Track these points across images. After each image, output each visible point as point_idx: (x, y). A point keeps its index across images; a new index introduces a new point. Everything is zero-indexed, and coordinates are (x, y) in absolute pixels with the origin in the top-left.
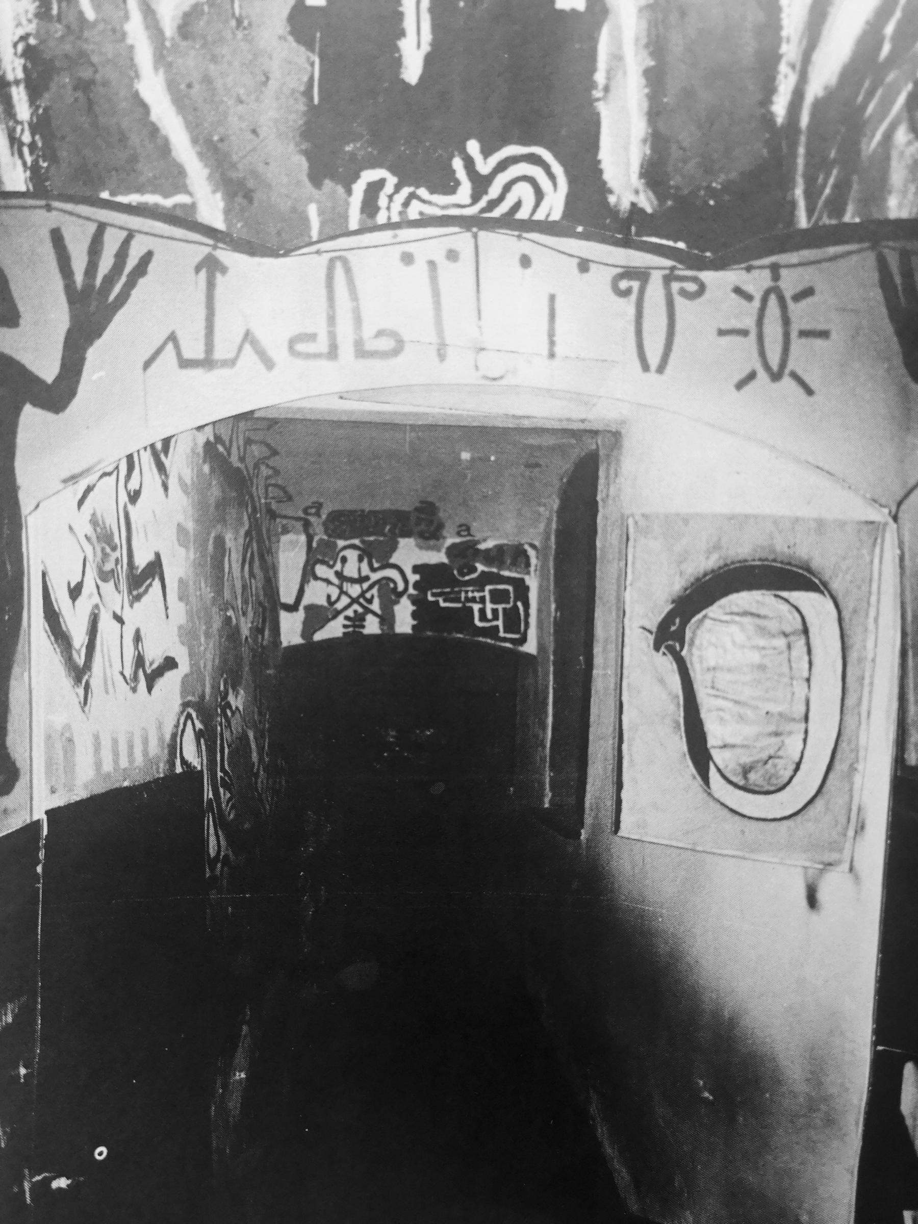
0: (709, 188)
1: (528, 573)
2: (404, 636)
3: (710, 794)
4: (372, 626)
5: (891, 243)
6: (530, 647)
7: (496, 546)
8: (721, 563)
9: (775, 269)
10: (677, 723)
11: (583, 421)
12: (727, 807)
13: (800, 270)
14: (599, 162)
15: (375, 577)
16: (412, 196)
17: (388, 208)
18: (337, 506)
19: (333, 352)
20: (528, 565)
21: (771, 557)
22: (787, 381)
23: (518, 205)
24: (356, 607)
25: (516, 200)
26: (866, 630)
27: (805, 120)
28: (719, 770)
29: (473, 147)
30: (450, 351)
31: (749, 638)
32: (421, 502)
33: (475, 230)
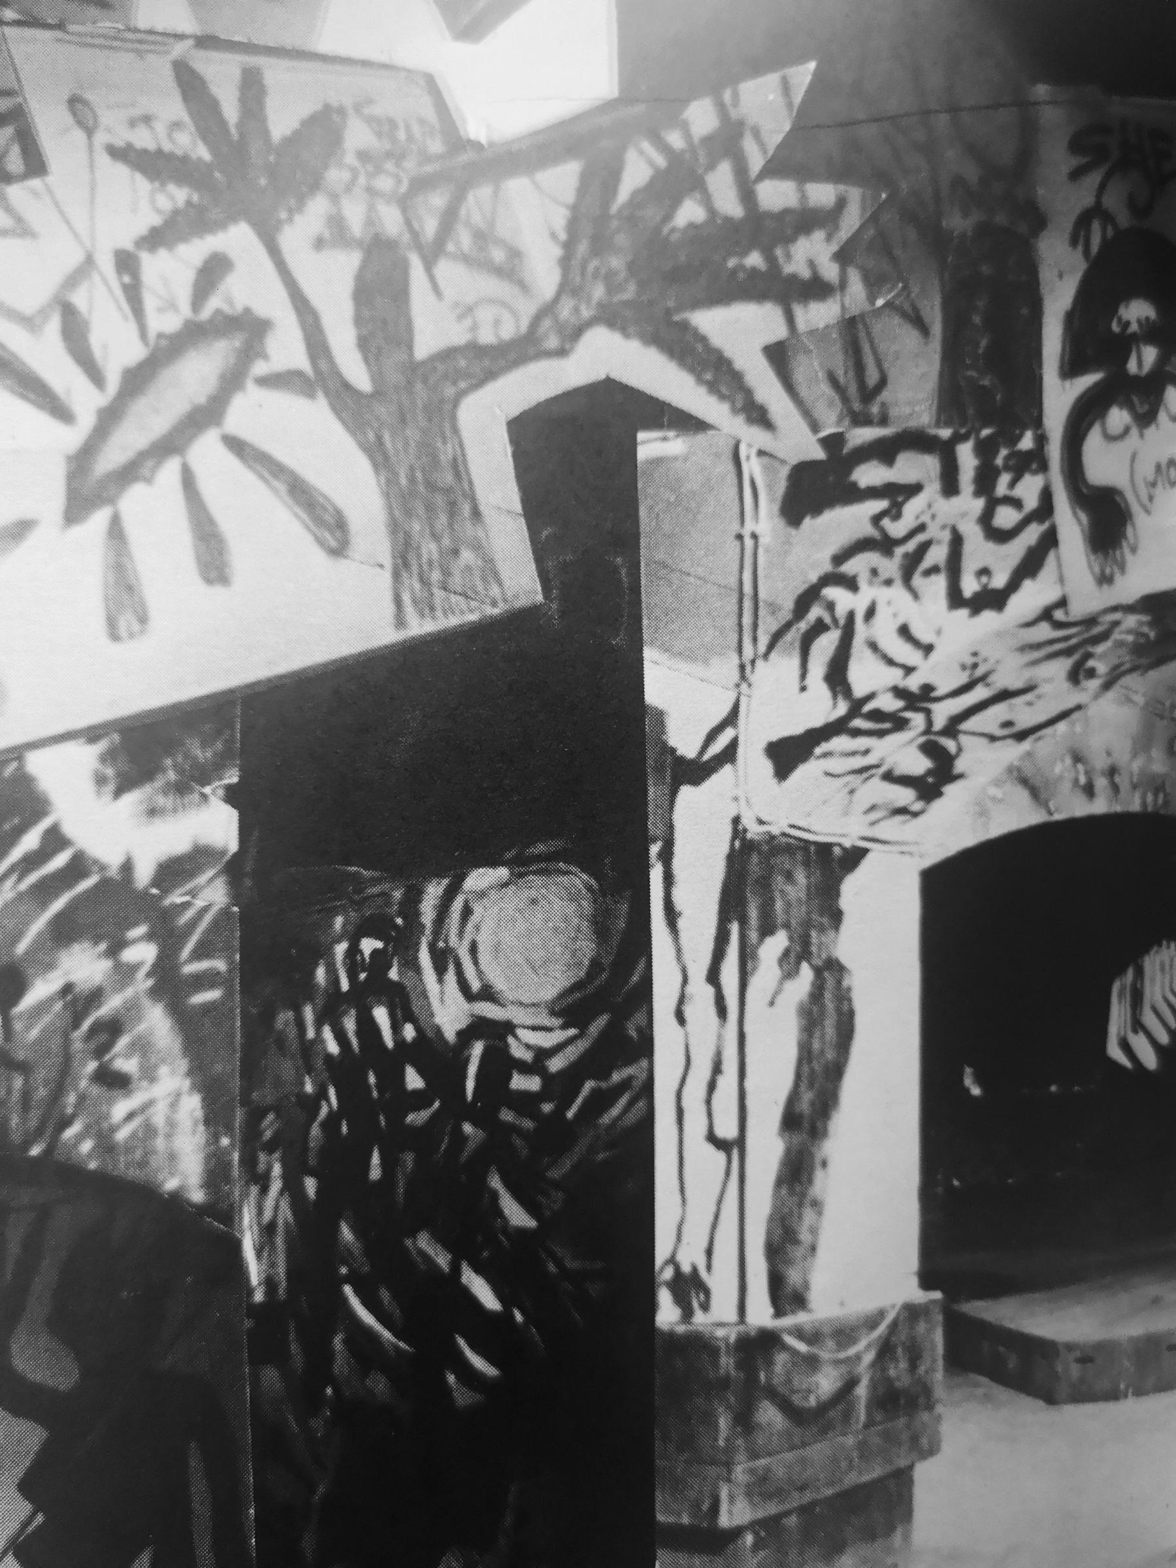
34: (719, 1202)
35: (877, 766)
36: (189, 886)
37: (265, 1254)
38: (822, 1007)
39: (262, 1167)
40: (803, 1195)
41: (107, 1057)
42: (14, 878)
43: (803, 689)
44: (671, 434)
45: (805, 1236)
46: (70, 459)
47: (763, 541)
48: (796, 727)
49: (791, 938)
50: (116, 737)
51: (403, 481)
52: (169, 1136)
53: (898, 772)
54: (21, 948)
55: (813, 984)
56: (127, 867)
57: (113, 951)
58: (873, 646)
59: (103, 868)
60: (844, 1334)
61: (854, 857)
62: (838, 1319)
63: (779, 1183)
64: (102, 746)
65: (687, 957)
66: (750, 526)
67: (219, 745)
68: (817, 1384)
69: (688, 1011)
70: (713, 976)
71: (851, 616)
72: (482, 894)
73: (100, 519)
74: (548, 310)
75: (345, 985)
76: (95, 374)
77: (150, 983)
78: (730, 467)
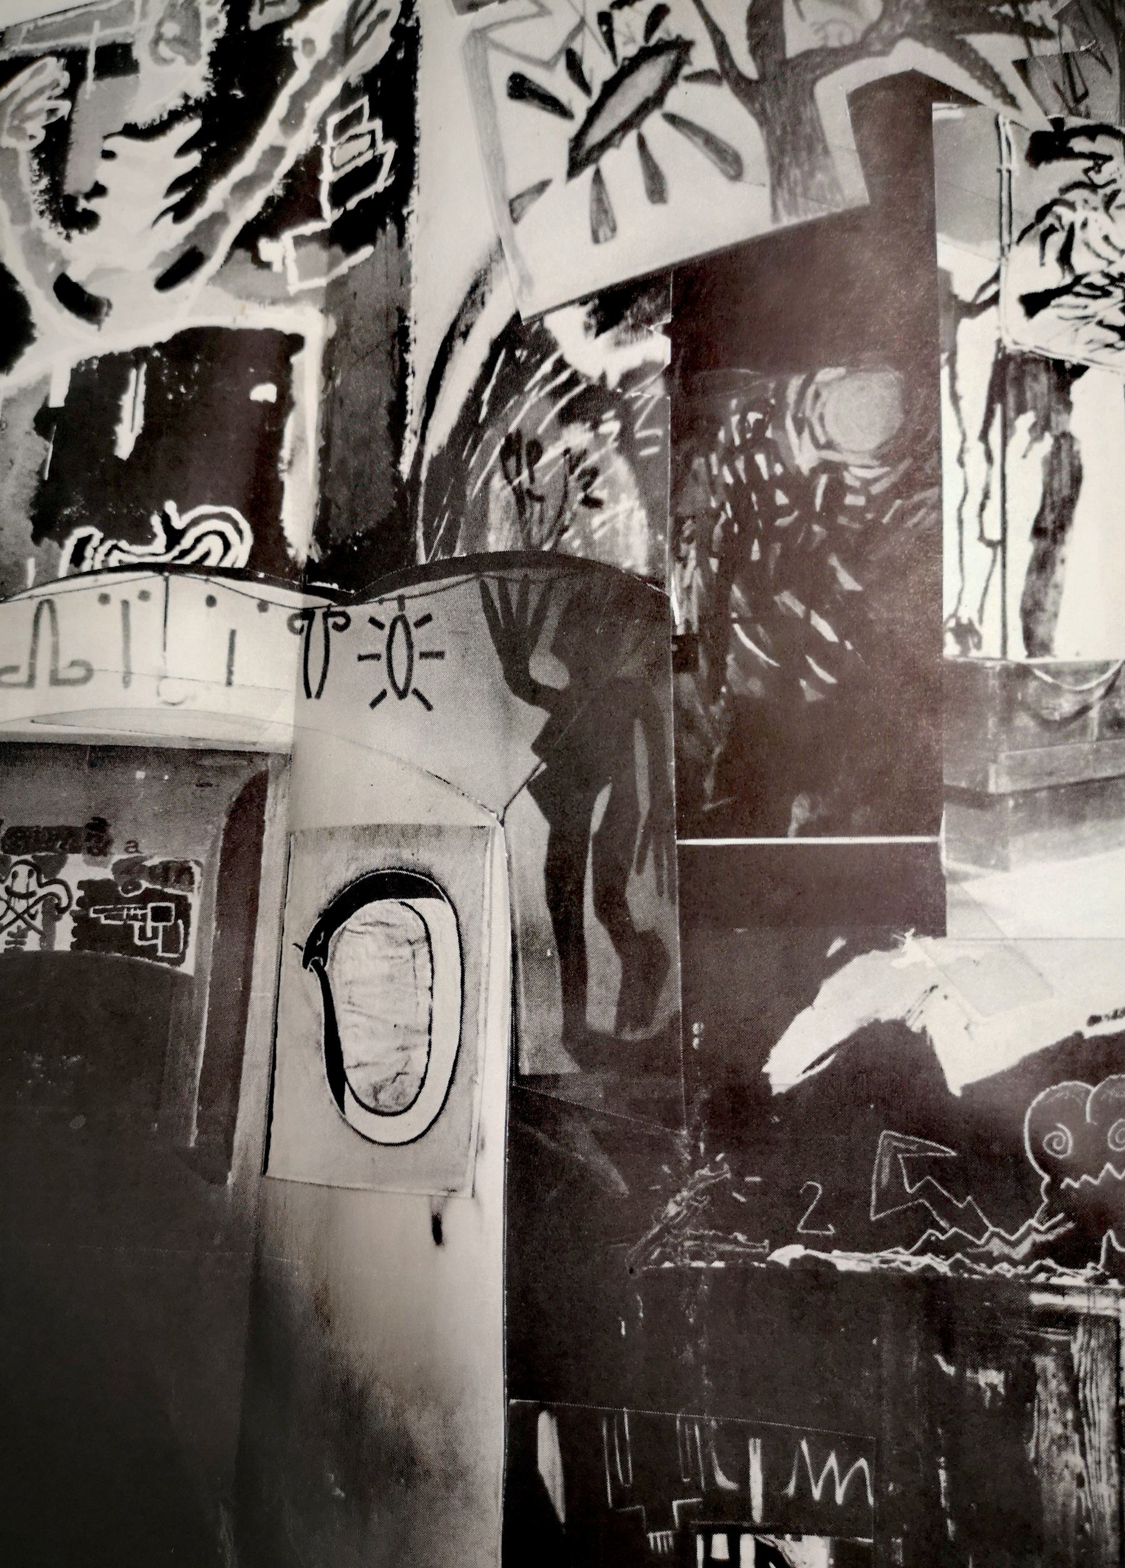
0: (355, 537)
1: (192, 891)
2: (61, 955)
3: (344, 1120)
4: (32, 943)
5: (492, 573)
6: (188, 968)
7: (161, 863)
8: (358, 874)
9: (401, 600)
10: (318, 1043)
11: (254, 744)
12: (359, 1133)
13: (421, 599)
14: (281, 521)
15: (41, 892)
16: (115, 547)
17: (93, 559)
18: (15, 824)
19: (31, 681)
20: (192, 882)
21: (399, 864)
22: (411, 698)
23: (207, 555)
24: (20, 923)
25: (206, 550)
26: (481, 933)
27: (423, 475)
28: (353, 1092)
29: (170, 507)
30: (134, 678)
31: (380, 948)
32: (94, 819)
33: (166, 574)
34: (988, 580)
35: (1093, 317)
36: (640, 386)
37: (685, 606)
38: (1060, 463)
39: (683, 553)
40: (1048, 579)
41: (589, 490)
42: (537, 389)
43: (1042, 264)
44: (955, 106)
45: (1049, 606)
46: (571, 141)
47: (1015, 175)
48: (1039, 288)
49: (1037, 416)
50: (597, 301)
51: (778, 132)
52: (626, 535)
53: (1106, 322)
54: (540, 430)
55: (1053, 446)
56: (603, 378)
57: (595, 426)
58: (1087, 245)
59: (588, 379)
60: (1081, 673)
61: (1079, 370)
62: (1075, 663)
63: (1030, 571)
64: (589, 306)
65: (966, 424)
66: (1005, 165)
67: (659, 301)
68: (1060, 705)
69: (967, 458)
70: (984, 436)
71: (1072, 226)
72: (827, 384)
73: (588, 173)
74: (874, 27)
75: (737, 442)
76: (586, 88)
77: (616, 444)
78: (993, 127)
